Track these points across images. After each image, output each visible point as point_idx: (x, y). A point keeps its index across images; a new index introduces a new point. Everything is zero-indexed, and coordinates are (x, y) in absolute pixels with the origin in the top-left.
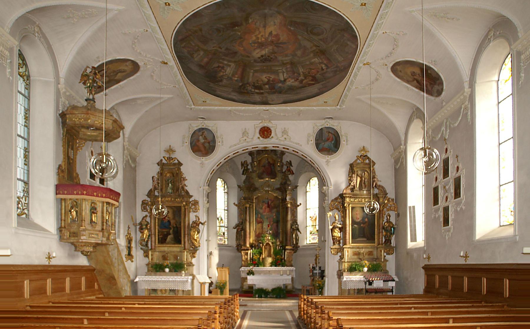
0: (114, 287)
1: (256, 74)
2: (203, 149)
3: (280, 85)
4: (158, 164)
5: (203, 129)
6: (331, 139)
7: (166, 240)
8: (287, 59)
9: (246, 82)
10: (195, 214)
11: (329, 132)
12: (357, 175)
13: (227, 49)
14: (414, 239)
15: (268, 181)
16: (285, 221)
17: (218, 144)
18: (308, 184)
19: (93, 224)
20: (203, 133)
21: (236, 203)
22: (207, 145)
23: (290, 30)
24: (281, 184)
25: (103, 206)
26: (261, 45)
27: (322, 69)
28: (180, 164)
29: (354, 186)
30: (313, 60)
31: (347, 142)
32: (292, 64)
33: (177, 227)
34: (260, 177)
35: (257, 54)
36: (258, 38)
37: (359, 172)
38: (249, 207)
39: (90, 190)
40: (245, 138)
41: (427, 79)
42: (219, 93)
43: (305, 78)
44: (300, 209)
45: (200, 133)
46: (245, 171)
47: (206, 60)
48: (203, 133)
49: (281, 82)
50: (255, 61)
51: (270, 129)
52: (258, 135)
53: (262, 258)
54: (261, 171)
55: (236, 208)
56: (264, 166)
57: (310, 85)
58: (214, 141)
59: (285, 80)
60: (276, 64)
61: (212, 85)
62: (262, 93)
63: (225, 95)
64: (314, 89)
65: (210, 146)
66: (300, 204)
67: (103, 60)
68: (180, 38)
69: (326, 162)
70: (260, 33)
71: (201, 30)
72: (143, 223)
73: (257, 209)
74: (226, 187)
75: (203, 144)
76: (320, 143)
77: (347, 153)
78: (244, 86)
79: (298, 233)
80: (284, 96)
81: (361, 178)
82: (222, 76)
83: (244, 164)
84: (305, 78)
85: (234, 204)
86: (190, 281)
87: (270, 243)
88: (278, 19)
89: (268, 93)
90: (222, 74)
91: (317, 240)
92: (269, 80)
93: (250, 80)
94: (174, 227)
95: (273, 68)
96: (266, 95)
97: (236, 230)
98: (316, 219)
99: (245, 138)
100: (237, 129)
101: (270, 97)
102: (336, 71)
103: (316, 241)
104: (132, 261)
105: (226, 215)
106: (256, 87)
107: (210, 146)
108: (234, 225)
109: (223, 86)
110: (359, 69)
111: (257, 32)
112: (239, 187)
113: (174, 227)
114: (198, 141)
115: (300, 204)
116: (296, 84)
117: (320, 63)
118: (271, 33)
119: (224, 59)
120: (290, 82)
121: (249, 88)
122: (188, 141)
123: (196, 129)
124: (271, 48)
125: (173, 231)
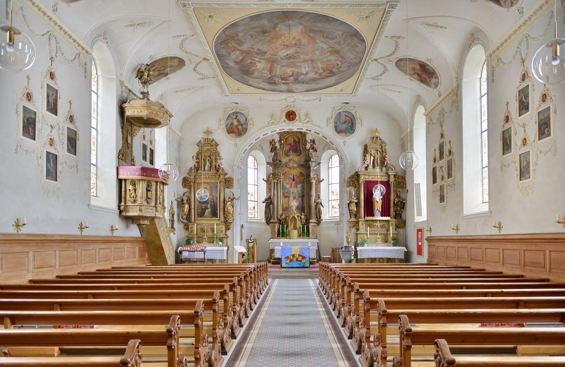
0: (162, 256)
1: (283, 69)
2: (236, 131)
3: (303, 77)
4: (198, 145)
5: (237, 113)
7: (204, 214)
8: (308, 57)
9: (274, 75)
10: (230, 190)
12: (371, 155)
13: (258, 49)
14: (420, 214)
15: (294, 155)
16: (310, 196)
17: (249, 126)
19: (148, 200)
20: (237, 116)
21: (265, 179)
23: (309, 36)
25: (157, 185)
26: (287, 47)
27: (338, 65)
28: (217, 145)
29: (368, 165)
30: (329, 58)
32: (312, 61)
35: (283, 53)
36: (284, 42)
37: (373, 152)
38: (277, 183)
39: (149, 172)
40: (273, 121)
41: (424, 73)
42: (250, 83)
43: (324, 72)
45: (234, 117)
46: (274, 149)
47: (241, 58)
48: (237, 116)
49: (303, 74)
50: (282, 59)
51: (294, 112)
52: (284, 118)
54: (287, 148)
55: (265, 183)
56: (291, 144)
57: (328, 77)
58: (246, 124)
59: (307, 73)
60: (299, 61)
61: (245, 77)
62: (288, 84)
63: (255, 84)
64: (332, 80)
65: (243, 128)
67: (318, 313)
68: (220, 41)
70: (285, 38)
71: (237, 36)
73: (284, 184)
75: (237, 127)
77: (361, 134)
78: (272, 77)
79: (321, 207)
80: (307, 85)
81: (374, 157)
82: (254, 70)
83: (272, 142)
84: (324, 72)
86: (225, 252)
87: (296, 216)
88: (300, 28)
89: (293, 83)
90: (253, 68)
92: (293, 73)
93: (278, 73)
95: (297, 64)
96: (291, 84)
97: (265, 204)
99: (273, 121)
100: (266, 113)
101: (294, 87)
102: (349, 66)
103: (386, 180)
104: (174, 234)
105: (256, 189)
106: (282, 79)
107: (243, 128)
108: (263, 200)
109: (254, 77)
110: (368, 64)
111: (283, 38)
112: (268, 163)
113: (211, 202)
114: (232, 124)
116: (317, 76)
117: (335, 60)
118: (294, 38)
119: (256, 57)
120: (311, 75)
121: (277, 80)
122: (223, 123)
123: (230, 112)
124: (294, 48)
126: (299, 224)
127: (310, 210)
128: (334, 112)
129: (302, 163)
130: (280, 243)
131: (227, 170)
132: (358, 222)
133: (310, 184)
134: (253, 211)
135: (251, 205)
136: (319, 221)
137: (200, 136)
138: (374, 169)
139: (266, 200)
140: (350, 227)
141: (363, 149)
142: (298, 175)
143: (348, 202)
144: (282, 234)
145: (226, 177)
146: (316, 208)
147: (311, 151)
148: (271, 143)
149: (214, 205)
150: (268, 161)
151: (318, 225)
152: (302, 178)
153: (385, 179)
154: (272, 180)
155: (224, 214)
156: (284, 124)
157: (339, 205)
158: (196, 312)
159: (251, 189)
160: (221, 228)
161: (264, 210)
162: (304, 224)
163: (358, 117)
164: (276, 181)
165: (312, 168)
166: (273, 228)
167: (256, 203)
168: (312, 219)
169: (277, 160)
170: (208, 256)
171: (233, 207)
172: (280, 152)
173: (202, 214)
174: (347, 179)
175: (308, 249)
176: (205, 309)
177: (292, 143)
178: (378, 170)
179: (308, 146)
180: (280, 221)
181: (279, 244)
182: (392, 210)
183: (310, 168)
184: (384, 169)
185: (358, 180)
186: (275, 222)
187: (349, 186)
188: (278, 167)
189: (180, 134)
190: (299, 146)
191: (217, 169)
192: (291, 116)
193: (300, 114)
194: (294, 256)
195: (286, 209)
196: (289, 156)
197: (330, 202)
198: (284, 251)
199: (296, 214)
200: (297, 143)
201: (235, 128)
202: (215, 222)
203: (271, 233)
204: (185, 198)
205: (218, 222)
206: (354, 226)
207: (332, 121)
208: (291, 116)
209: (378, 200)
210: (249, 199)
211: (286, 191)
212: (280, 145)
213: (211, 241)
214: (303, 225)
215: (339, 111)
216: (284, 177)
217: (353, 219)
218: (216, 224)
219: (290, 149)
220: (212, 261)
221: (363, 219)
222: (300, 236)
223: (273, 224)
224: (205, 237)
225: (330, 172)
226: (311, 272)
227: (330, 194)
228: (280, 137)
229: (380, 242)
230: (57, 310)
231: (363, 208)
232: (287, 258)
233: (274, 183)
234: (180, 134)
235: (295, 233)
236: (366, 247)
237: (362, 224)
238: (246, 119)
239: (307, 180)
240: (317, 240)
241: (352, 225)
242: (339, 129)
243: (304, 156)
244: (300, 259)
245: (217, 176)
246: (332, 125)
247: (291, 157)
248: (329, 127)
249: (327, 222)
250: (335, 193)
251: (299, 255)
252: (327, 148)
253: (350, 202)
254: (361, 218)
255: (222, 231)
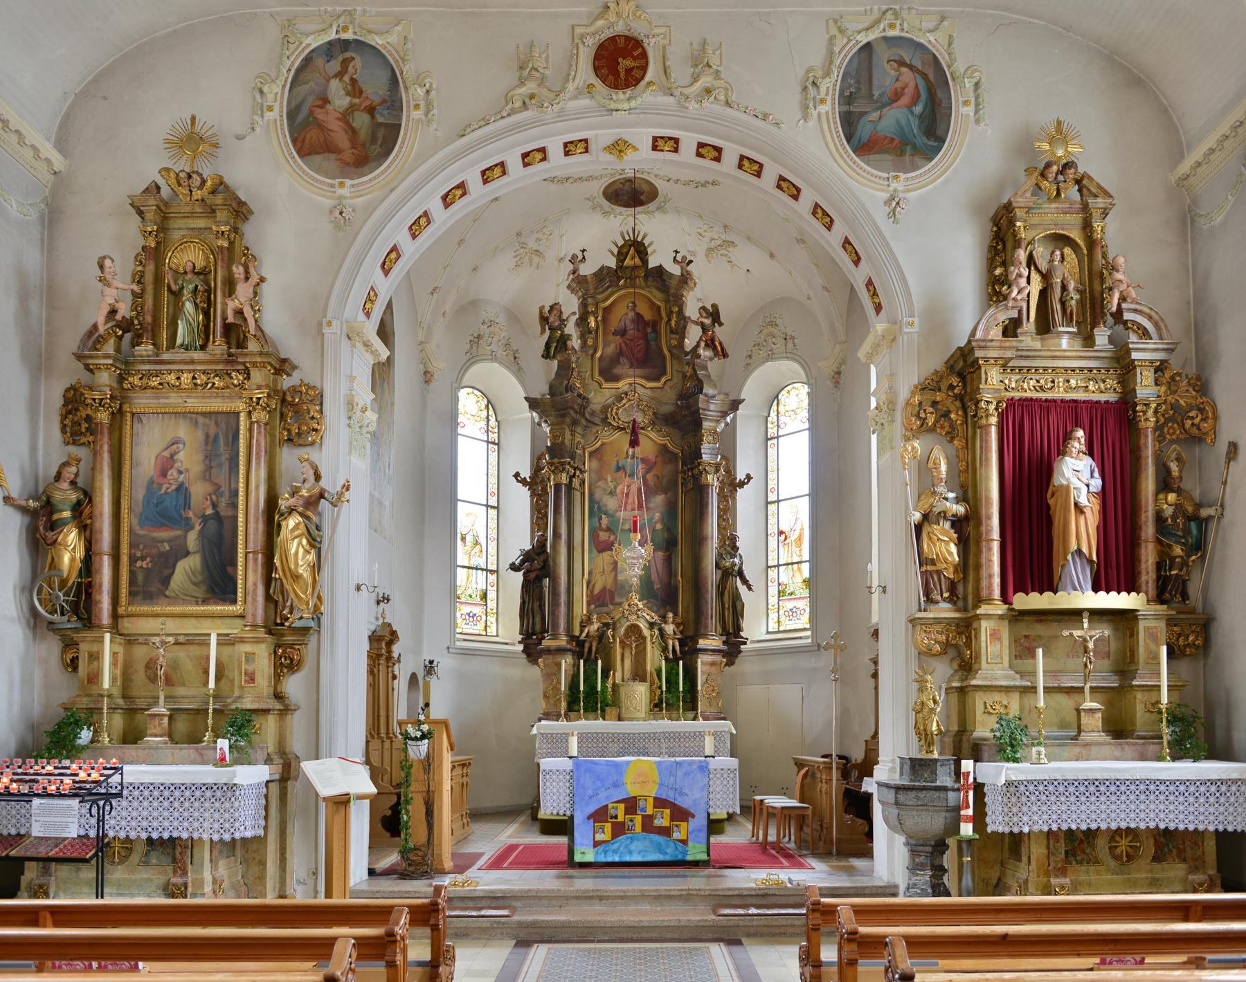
2: (342, 140)
5: (345, 45)
6: (909, 91)
7: (166, 581)
11: (902, 63)
16: (698, 540)
17: (411, 117)
18: (774, 407)
20: (345, 63)
22: (361, 121)
24: (681, 396)
31: (977, 105)
33: (217, 516)
34: (609, 374)
40: (531, 87)
44: (745, 499)
45: (335, 66)
46: (556, 346)
48: (345, 63)
52: (585, 72)
53: (614, 685)
54: (611, 349)
55: (525, 492)
56: (622, 332)
58: (394, 103)
66: (749, 477)
69: (887, 202)
72: (57, 496)
73: (598, 495)
74: (492, 419)
76: (863, 114)
77: (977, 152)
79: (742, 589)
83: (550, 319)
85: (517, 475)
87: (643, 625)
91: (806, 617)
94: (205, 519)
97: (519, 577)
98: (800, 538)
99: (531, 87)
103: (1111, 397)
105: (493, 524)
107: (376, 126)
108: (515, 556)
112: (533, 404)
113: (205, 519)
115: (749, 477)
122: (277, 93)
123: (315, 42)
125: (201, 533)
126: (654, 658)
127: (698, 594)
128: (841, 41)
129: (667, 409)
130: (565, 737)
131: (290, 343)
132: (966, 627)
133: (701, 491)
134: (478, 610)
135: (469, 583)
136: (733, 648)
137: (148, 163)
138: (1051, 341)
139: (527, 557)
140: (925, 654)
141: (988, 236)
142: (652, 457)
143: (917, 516)
144: (587, 699)
145: (286, 382)
146: (721, 594)
147: (705, 353)
148: (544, 319)
149: (220, 536)
150: (536, 395)
151: (730, 663)
152: (669, 468)
153: (1103, 392)
154: (552, 479)
155: (268, 581)
156: (585, 102)
157: (808, 583)
158: (391, 934)
159: (471, 518)
160: (250, 657)
161: (518, 601)
162: (676, 660)
163: (960, 67)
164: (564, 478)
165: (706, 424)
166: (551, 675)
167: (492, 578)
168: (705, 636)
169: (569, 389)
170: (124, 822)
171: (314, 543)
172: (585, 368)
173: (149, 583)
174: (903, 393)
175: (703, 768)
176: (413, 922)
177: (630, 326)
178: (1065, 341)
179: (693, 336)
180: (581, 644)
181: (558, 745)
182: (1148, 556)
183: (698, 424)
184: (1102, 337)
185: (967, 398)
186: (561, 651)
187: (924, 429)
188: (575, 423)
189: (58, 161)
190: (658, 339)
191: (234, 333)
192: (624, 63)
193: (667, 46)
194: (631, 804)
195: (602, 599)
196: (616, 379)
197: (772, 574)
198: (587, 780)
199: (641, 614)
200: (647, 328)
201: (335, 125)
202: (214, 627)
203: (546, 696)
204: (66, 496)
205: (234, 628)
206: (946, 646)
207: (830, 85)
208: (624, 63)
209: (1083, 500)
210: (462, 559)
211: (605, 521)
212: (583, 337)
213: (189, 730)
214: (672, 663)
215: (864, 39)
216: (595, 464)
217: (944, 611)
218: (212, 640)
219: (620, 353)
220: (171, 851)
221: (999, 608)
222: (658, 705)
223: (550, 659)
224: (161, 709)
225: (772, 452)
226: (722, 899)
227: (773, 542)
228: (584, 305)
229: (1103, 737)
230: (45, 926)
231: (996, 546)
232: (600, 815)
233: (557, 487)
234: (58, 161)
235: (640, 693)
236: (1038, 766)
237: (995, 636)
238: (394, 81)
239: (689, 483)
240: (728, 726)
241: (933, 640)
242: (864, 130)
243: (677, 379)
244: (663, 820)
245: (237, 378)
246: (829, 108)
247: (623, 385)
248: (812, 123)
249: (760, 653)
250: (793, 537)
251: (660, 803)
252: (763, 353)
253: (926, 517)
254: (989, 601)
255: (251, 678)
